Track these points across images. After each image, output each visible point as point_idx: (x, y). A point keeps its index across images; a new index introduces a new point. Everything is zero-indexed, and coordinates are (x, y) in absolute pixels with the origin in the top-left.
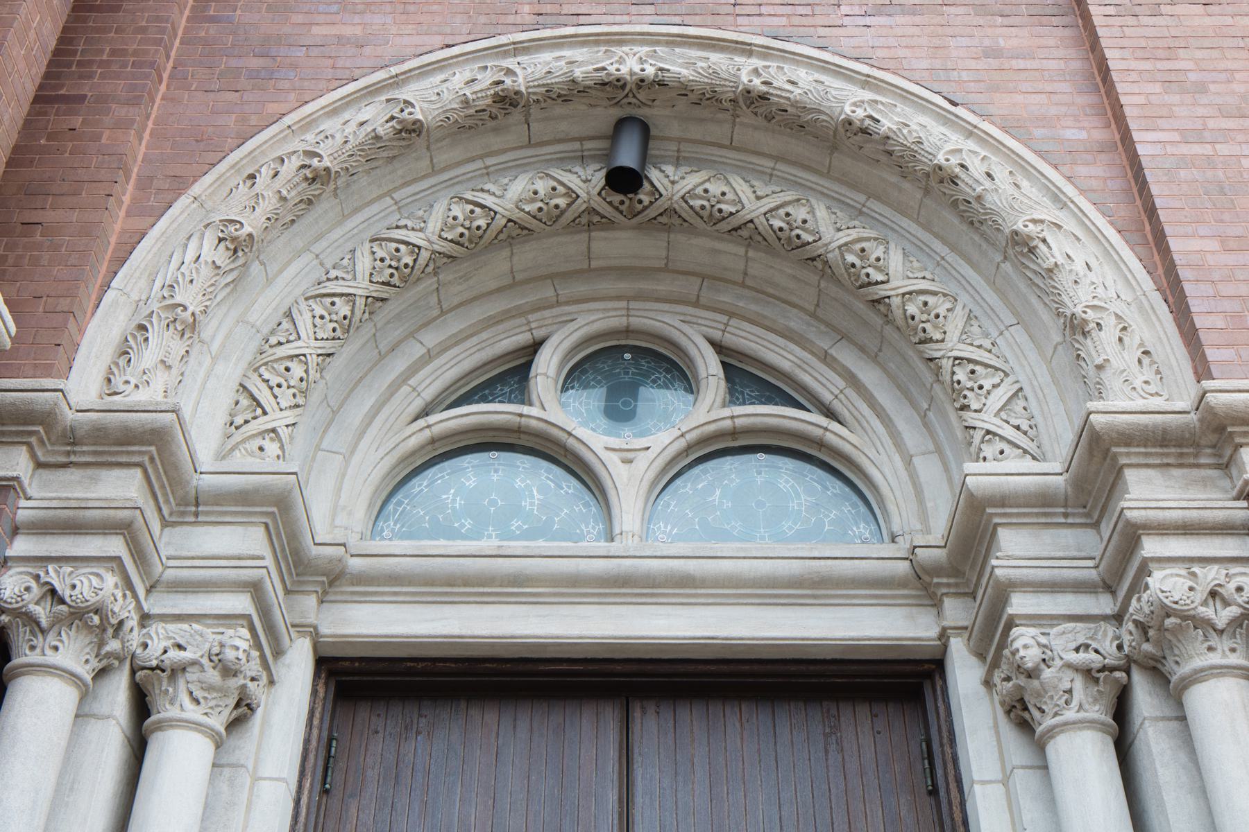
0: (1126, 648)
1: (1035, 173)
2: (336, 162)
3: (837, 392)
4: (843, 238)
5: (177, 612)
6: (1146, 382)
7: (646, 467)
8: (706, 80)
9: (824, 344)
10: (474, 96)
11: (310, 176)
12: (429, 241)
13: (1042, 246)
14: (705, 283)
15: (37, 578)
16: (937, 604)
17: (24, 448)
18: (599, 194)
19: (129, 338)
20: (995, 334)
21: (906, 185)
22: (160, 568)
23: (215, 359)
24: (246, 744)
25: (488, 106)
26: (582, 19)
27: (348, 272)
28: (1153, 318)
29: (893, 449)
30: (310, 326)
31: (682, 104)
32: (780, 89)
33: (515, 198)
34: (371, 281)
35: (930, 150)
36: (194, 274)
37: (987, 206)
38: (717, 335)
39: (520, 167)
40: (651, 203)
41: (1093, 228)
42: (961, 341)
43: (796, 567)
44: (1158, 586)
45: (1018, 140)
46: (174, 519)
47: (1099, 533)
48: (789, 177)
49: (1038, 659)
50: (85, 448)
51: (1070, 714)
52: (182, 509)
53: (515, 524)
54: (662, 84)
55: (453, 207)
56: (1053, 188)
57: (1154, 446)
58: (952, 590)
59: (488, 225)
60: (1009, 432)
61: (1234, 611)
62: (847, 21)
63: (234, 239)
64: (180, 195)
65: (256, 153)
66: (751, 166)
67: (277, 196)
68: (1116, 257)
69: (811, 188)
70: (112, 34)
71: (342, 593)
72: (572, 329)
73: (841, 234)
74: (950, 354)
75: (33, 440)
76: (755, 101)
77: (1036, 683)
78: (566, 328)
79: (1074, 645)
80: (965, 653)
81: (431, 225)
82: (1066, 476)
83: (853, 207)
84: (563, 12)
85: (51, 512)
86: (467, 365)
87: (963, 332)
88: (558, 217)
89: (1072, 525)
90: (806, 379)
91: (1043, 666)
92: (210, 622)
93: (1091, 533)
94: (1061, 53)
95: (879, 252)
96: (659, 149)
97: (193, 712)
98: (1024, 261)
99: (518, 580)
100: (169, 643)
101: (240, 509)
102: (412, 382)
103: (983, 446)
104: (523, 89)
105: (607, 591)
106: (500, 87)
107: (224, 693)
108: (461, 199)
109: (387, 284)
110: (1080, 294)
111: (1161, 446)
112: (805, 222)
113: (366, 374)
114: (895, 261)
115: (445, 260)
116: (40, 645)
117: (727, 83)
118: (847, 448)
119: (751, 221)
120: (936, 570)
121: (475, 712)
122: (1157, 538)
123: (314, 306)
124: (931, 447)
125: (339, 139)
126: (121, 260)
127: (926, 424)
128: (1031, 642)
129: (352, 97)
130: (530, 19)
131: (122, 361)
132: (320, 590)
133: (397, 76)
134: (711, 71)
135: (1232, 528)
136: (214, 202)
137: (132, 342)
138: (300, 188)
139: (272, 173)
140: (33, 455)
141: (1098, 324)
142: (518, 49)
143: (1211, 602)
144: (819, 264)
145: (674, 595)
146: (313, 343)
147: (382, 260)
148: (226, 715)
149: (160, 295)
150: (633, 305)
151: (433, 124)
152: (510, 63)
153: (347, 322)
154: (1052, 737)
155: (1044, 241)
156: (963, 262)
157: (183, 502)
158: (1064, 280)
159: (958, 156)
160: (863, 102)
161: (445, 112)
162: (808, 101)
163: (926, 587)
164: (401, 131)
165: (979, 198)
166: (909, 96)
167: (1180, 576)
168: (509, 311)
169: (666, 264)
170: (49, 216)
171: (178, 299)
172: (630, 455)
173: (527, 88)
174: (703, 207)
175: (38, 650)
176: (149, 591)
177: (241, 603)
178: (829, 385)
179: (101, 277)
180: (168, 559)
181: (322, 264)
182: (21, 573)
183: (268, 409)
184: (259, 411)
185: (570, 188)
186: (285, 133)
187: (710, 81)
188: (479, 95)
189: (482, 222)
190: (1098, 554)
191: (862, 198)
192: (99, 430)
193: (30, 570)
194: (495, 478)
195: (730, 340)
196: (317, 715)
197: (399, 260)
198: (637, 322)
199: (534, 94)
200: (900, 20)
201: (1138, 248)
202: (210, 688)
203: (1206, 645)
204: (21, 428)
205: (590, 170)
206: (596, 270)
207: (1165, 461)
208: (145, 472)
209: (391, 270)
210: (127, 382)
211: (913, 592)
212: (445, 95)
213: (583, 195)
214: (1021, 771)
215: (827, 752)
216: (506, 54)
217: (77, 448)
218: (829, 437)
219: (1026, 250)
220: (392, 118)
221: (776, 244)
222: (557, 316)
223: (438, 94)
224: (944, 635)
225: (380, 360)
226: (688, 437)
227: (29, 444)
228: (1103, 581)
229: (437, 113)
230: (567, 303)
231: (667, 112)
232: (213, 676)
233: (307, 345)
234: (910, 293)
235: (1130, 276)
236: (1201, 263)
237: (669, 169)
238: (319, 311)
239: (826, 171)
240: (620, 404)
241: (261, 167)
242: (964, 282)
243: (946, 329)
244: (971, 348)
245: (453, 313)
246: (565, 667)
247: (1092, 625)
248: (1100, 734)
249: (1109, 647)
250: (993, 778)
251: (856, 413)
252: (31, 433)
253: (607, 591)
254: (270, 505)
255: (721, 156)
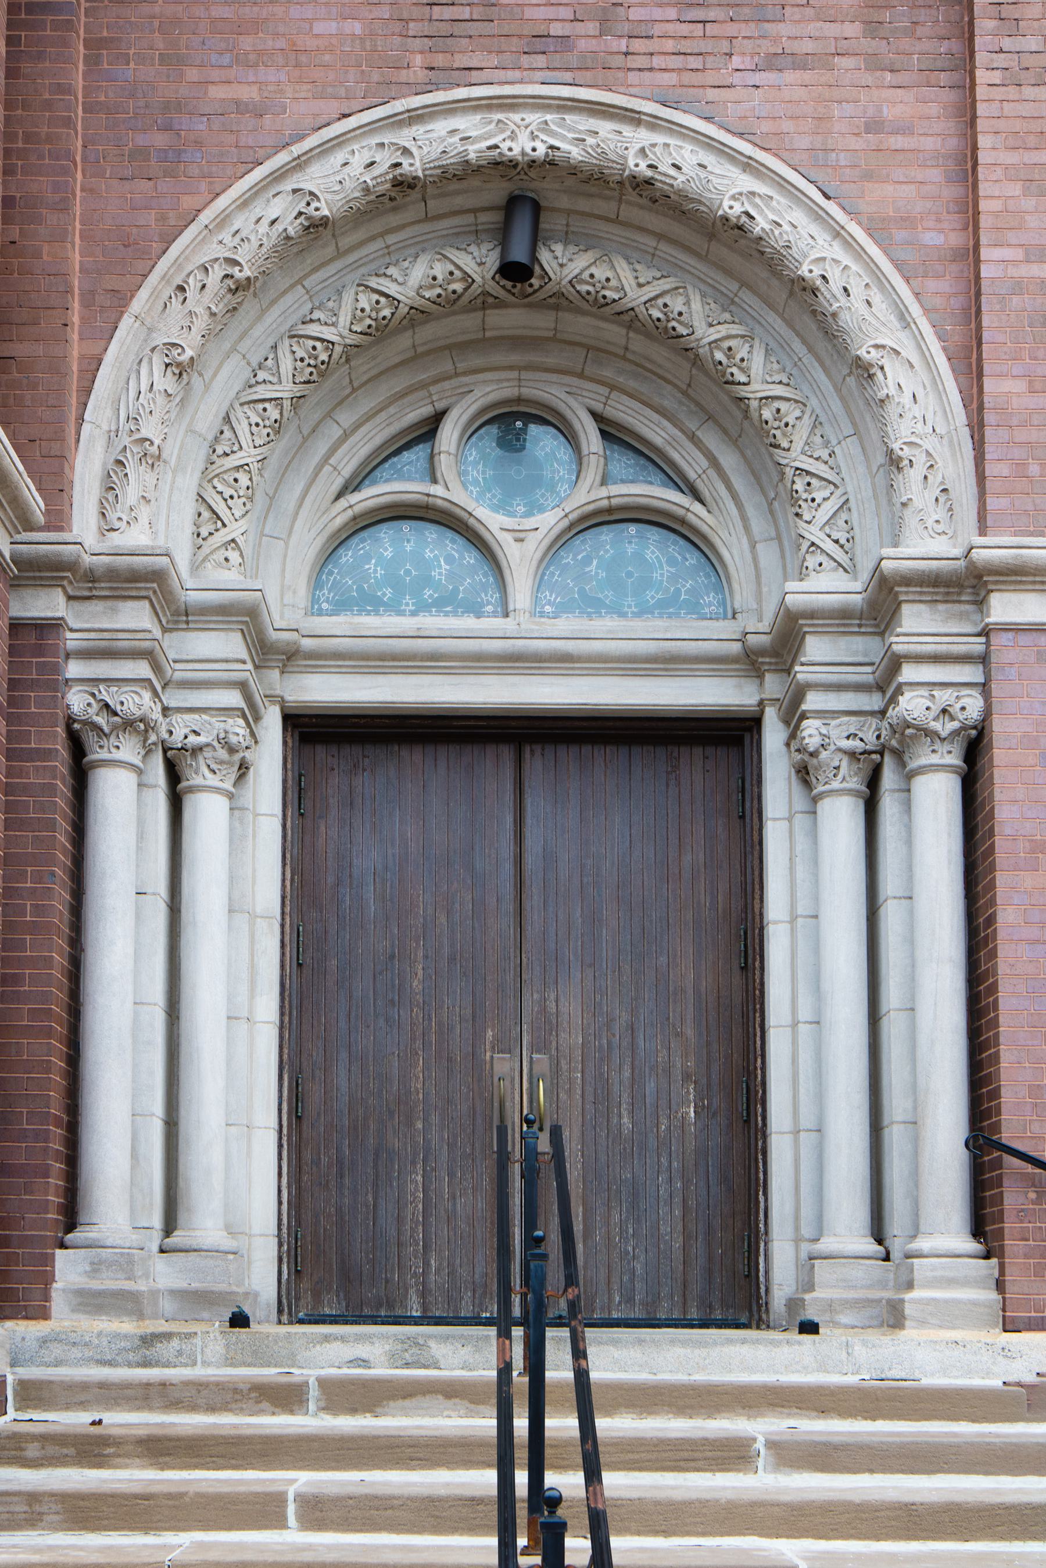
0: (882, 740)
1: (888, 286)
2: (254, 268)
3: (700, 472)
4: (714, 334)
5: (189, 706)
6: (937, 521)
7: (534, 546)
8: (594, 161)
9: (692, 425)
10: (374, 182)
11: (233, 287)
12: (341, 336)
13: (879, 374)
14: (589, 355)
15: (93, 695)
16: (760, 677)
17: (60, 589)
18: (493, 278)
19: (111, 473)
20: (834, 442)
21: (775, 282)
22: (170, 672)
23: (175, 472)
24: (247, 795)
25: (388, 190)
26: (475, 76)
27: (273, 374)
28: (958, 454)
29: (743, 531)
30: (249, 435)
31: (570, 182)
32: (665, 175)
33: (416, 286)
34: (294, 383)
35: (797, 257)
36: (152, 405)
37: (840, 324)
38: (598, 407)
39: (418, 248)
40: (541, 287)
41: (927, 354)
42: (803, 453)
43: (652, 647)
44: (905, 706)
45: (879, 245)
46: (170, 626)
47: (883, 641)
48: (670, 258)
49: (817, 745)
50: (103, 585)
51: (835, 785)
52: (175, 618)
53: (428, 592)
54: (552, 163)
55: (361, 296)
56: (901, 306)
57: (928, 586)
58: (773, 667)
59: (393, 314)
60: (829, 546)
61: (956, 725)
62: (737, 78)
63: (179, 365)
64: (122, 313)
65: (181, 260)
66: (635, 244)
67: (208, 313)
68: (940, 387)
69: (689, 272)
70: (19, 112)
71: (298, 666)
72: (469, 402)
73: (712, 330)
74: (793, 464)
75: (65, 583)
76: (641, 185)
77: (815, 761)
78: (464, 401)
79: (846, 734)
80: (775, 719)
81: (341, 319)
82: (864, 595)
83: (726, 295)
84: (455, 66)
85: (91, 643)
86: (378, 440)
87: (807, 443)
88: (455, 301)
89: (864, 633)
90: (675, 456)
91: (821, 749)
92: (214, 712)
93: (877, 639)
94: (938, 127)
95: (743, 353)
96: (549, 223)
97: (212, 780)
98: (864, 383)
99: (434, 657)
100: (187, 731)
101: (220, 618)
102: (332, 461)
103: (807, 556)
104: (420, 174)
105: (504, 665)
106: (399, 171)
107: (230, 764)
108: (367, 287)
109: (308, 382)
110: (902, 428)
111: (934, 586)
112: (680, 314)
113: (293, 458)
114: (757, 363)
115: (356, 349)
116: (106, 745)
117: (615, 165)
118: (705, 529)
119: (632, 309)
120: (762, 652)
121: (405, 752)
122: (914, 665)
123: (249, 413)
124: (773, 534)
125: (255, 244)
126: (87, 391)
127: (772, 512)
128: (814, 732)
129: (260, 186)
130: (422, 75)
131: (110, 496)
132: (280, 665)
133: (299, 157)
134: (599, 151)
135: (971, 658)
136: (152, 318)
137: (115, 478)
138: (225, 301)
139: (199, 285)
140: (65, 592)
141: (911, 461)
142: (414, 117)
143: (941, 717)
144: (690, 354)
145: (556, 668)
146: (253, 451)
147: (302, 360)
148: (233, 777)
149: (127, 428)
150: (525, 375)
151: (338, 215)
152: (404, 137)
153: (277, 425)
154: (821, 799)
155: (882, 368)
156: (816, 364)
157: (175, 613)
158: (892, 410)
159: (821, 264)
160: (741, 194)
161: (347, 202)
162: (690, 190)
163: (753, 663)
164: (308, 228)
165: (834, 315)
166: (786, 185)
167: (922, 696)
168: (411, 385)
169: (555, 335)
170: (18, 349)
171: (144, 433)
172: (521, 535)
173: (424, 170)
174: (588, 293)
175: (106, 749)
176: (163, 688)
177: (233, 698)
178: (694, 464)
179: (74, 409)
180: (175, 662)
181: (249, 364)
182: (80, 691)
183: (226, 521)
184: (219, 523)
185: (466, 273)
186: (203, 234)
187: (598, 162)
188: (379, 180)
189: (387, 312)
190: (877, 661)
191: (734, 286)
192: (112, 571)
193: (86, 688)
194: (408, 549)
195: (610, 412)
196: (289, 760)
197: (316, 358)
198: (527, 392)
199: (431, 176)
200: (789, 76)
201: (962, 379)
202: (222, 762)
203: (931, 748)
204: (55, 574)
205: (486, 247)
206: (490, 339)
207: (935, 598)
208: (151, 602)
209: (311, 369)
210: (120, 519)
211: (743, 667)
212: (348, 184)
213: (478, 279)
214: (801, 815)
215: (667, 785)
216: (400, 124)
217: (97, 585)
218: (690, 517)
219: (866, 375)
220: (300, 214)
221: (655, 332)
222: (455, 388)
223: (340, 182)
224: (761, 703)
225: (303, 443)
226: (571, 517)
227: (63, 587)
228: (877, 684)
229: (340, 204)
230: (465, 373)
231: (557, 186)
232: (223, 754)
233: (248, 455)
234: (767, 398)
235: (948, 409)
236: (1006, 406)
237: (558, 248)
238: (255, 419)
239: (704, 254)
240: (512, 473)
241: (189, 275)
242: (815, 386)
243: (792, 437)
244: (811, 460)
245: (363, 389)
246: (472, 723)
247: (862, 719)
248: (854, 799)
249: (870, 737)
250: (781, 816)
251: (715, 494)
252: (63, 578)
253: (504, 665)
254: (243, 616)
255: (607, 232)
